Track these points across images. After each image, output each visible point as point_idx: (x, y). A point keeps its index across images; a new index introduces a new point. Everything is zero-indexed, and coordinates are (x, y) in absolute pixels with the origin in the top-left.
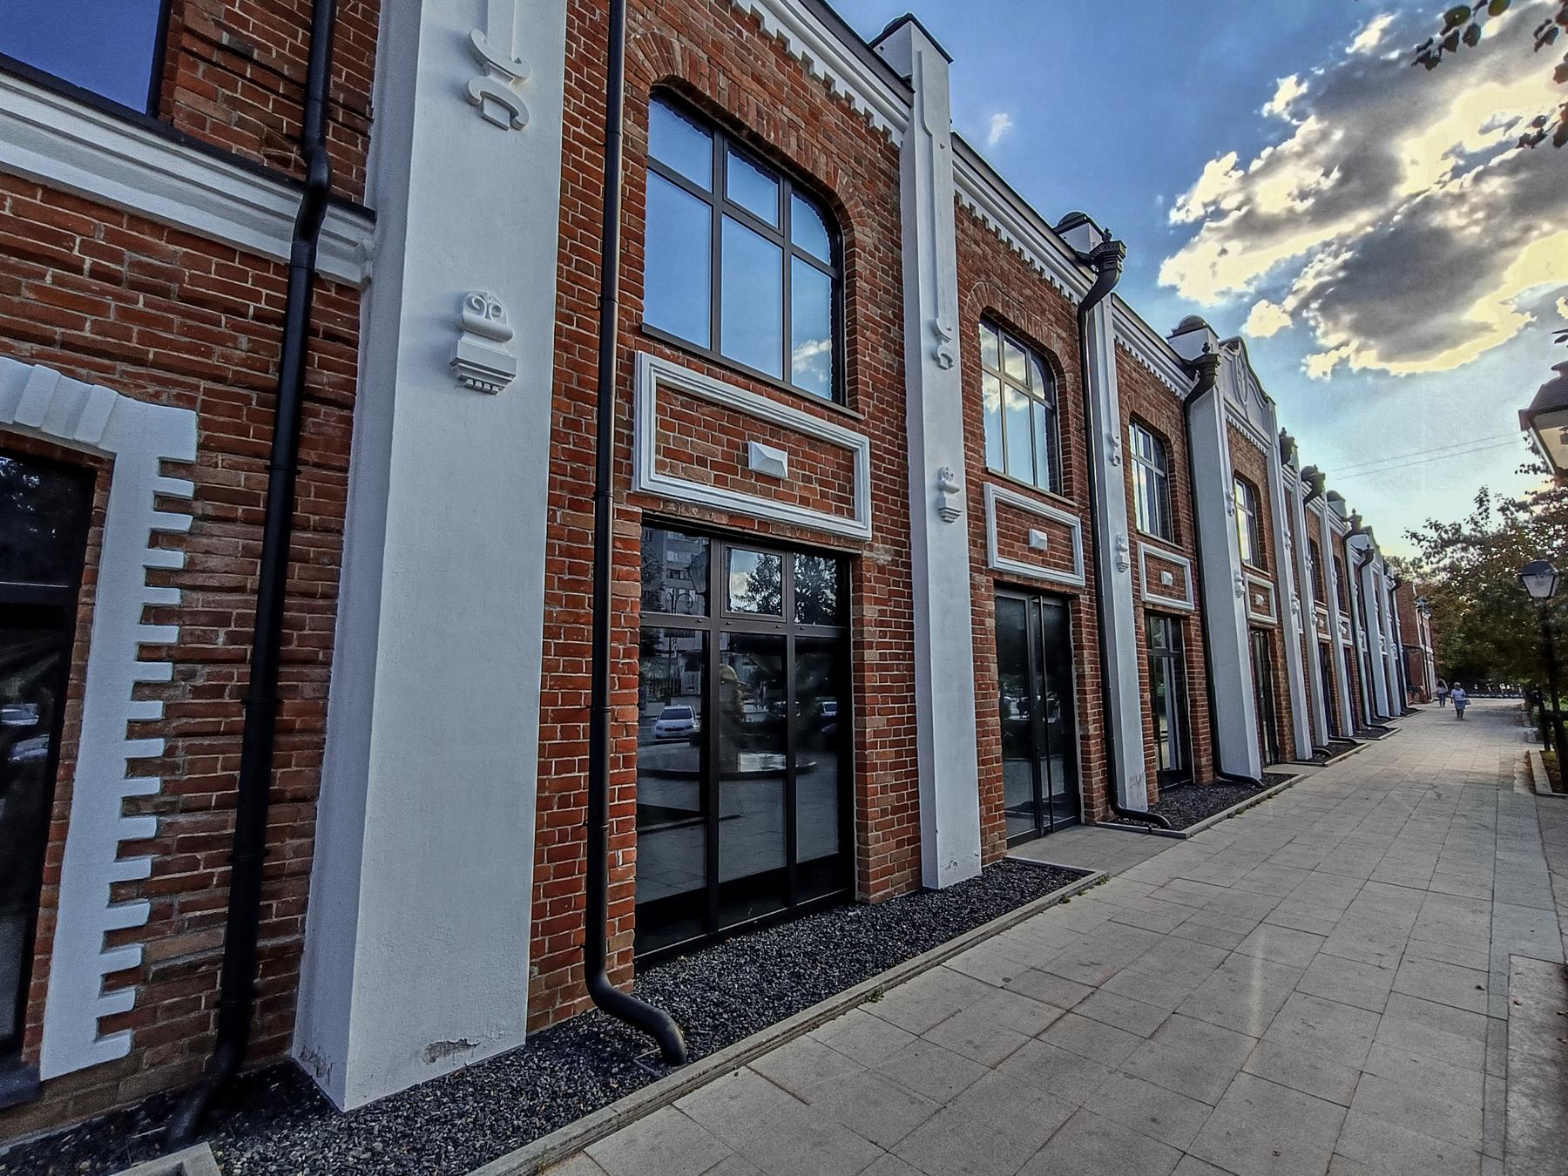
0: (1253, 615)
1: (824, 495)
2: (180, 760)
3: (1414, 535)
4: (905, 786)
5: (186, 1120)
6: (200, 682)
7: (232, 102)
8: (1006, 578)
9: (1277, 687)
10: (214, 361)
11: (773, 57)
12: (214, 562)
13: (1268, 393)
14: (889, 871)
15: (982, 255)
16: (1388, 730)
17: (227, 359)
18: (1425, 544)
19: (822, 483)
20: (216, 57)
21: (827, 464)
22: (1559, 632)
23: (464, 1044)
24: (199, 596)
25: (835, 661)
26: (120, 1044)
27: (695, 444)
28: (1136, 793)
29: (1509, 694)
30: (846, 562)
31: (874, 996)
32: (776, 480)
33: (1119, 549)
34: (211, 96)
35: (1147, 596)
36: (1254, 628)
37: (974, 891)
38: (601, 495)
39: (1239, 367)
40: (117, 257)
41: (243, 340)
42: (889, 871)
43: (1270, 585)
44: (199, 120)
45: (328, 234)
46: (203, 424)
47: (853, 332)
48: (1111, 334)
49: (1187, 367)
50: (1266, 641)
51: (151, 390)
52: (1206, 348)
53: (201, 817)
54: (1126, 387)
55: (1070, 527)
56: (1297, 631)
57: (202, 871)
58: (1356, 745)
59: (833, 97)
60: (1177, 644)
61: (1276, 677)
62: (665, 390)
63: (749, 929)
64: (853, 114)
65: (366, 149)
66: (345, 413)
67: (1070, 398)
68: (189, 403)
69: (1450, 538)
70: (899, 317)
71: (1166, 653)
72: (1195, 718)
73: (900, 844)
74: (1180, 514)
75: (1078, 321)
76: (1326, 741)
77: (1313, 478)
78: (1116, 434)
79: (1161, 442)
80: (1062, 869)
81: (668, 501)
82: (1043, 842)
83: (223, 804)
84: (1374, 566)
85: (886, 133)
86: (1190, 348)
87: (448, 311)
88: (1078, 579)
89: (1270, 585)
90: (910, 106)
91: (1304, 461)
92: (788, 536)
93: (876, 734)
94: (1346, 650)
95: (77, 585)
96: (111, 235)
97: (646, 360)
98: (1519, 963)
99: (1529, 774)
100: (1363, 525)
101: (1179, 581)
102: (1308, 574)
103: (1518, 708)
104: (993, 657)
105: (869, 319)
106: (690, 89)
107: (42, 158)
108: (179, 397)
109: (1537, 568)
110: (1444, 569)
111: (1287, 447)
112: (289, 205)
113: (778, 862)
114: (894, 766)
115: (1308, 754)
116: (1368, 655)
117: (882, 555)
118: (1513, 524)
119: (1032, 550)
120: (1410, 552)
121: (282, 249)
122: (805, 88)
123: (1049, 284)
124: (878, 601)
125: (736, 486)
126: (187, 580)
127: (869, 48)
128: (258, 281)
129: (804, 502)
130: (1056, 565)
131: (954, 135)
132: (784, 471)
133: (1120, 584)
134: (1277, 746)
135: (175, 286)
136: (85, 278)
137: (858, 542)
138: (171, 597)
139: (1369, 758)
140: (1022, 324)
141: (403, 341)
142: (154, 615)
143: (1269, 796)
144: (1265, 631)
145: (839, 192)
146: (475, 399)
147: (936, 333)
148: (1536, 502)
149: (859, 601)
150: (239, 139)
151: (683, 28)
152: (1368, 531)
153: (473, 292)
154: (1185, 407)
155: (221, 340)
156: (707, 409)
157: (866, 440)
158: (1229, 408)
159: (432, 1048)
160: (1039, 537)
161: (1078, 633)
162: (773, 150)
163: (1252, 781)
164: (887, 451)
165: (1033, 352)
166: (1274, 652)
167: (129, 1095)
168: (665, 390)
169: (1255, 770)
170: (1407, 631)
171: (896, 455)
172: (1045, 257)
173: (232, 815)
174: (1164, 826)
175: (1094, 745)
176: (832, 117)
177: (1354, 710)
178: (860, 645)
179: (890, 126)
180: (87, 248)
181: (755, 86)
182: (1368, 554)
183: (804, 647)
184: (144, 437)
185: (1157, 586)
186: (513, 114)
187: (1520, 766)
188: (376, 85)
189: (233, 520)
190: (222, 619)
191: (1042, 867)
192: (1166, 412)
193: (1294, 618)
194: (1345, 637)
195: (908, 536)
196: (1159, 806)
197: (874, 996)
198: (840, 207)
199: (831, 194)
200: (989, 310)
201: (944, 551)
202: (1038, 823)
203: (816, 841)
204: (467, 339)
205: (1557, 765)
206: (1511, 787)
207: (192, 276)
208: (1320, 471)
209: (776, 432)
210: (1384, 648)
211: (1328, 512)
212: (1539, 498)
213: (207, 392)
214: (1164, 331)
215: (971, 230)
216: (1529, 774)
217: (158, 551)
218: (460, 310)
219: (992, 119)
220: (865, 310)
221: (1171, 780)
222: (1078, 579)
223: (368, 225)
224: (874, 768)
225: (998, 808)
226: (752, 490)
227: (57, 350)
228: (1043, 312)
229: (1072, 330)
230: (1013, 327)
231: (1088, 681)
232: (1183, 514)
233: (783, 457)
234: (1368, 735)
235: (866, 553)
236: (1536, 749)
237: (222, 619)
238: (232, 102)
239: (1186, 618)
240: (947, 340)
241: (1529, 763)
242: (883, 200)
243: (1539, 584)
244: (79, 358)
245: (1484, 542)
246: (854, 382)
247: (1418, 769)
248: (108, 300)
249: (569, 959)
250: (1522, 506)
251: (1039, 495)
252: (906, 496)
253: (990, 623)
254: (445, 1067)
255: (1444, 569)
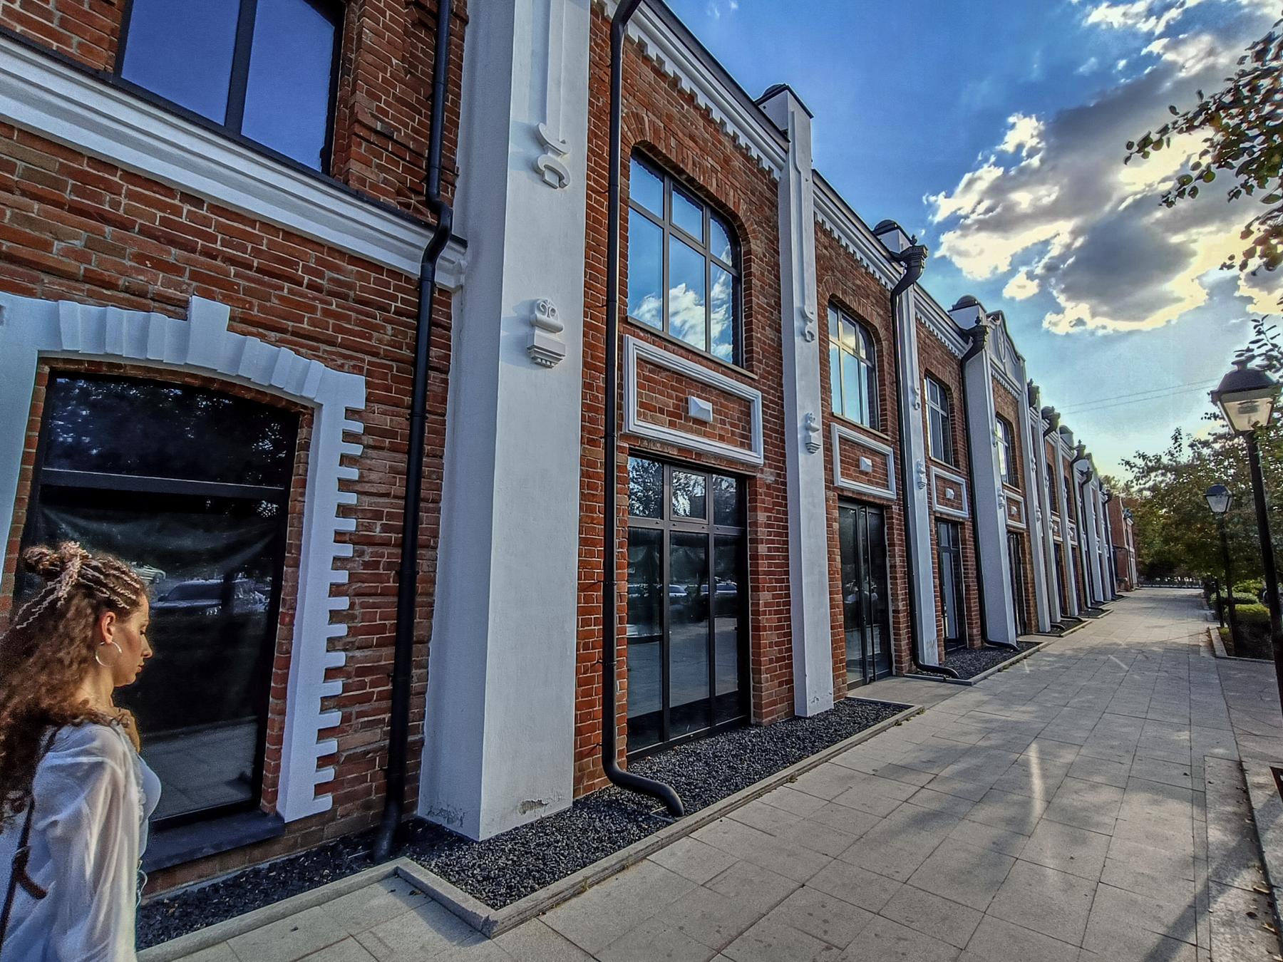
0: (1010, 522)
1: (733, 433)
2: (357, 612)
3: (1128, 463)
4: (782, 643)
5: (385, 845)
6: (367, 558)
7: (379, 166)
8: (845, 493)
9: (1026, 576)
10: (373, 343)
11: (701, 122)
12: (374, 476)
13: (1020, 349)
14: (774, 703)
15: (833, 261)
16: (1103, 611)
17: (380, 341)
18: (1136, 470)
19: (732, 425)
20: (373, 138)
21: (734, 410)
22: (1232, 538)
23: (540, 803)
24: (366, 499)
25: (738, 554)
26: (326, 802)
27: (660, 400)
28: (931, 653)
29: (1191, 585)
30: (744, 481)
31: (791, 779)
32: (704, 423)
33: (919, 472)
34: (368, 164)
35: (938, 508)
36: (1011, 532)
37: (832, 718)
38: (609, 436)
39: (999, 334)
40: (321, 276)
41: (389, 327)
42: (774, 703)
43: (1020, 499)
44: (362, 181)
45: (444, 259)
46: (368, 385)
47: (749, 316)
48: (913, 310)
49: (963, 334)
50: (1018, 539)
51: (340, 362)
52: (978, 321)
53: (368, 652)
54: (922, 349)
55: (884, 455)
56: (1040, 535)
57: (368, 690)
58: (1081, 622)
59: (738, 147)
60: (956, 543)
61: (1025, 569)
62: (642, 361)
63: (688, 740)
64: (748, 158)
65: (453, 195)
66: (443, 376)
67: (886, 360)
68: (359, 370)
69: (1153, 466)
70: (778, 304)
71: (947, 550)
72: (968, 599)
73: (781, 684)
74: (957, 444)
75: (891, 302)
76: (1059, 619)
77: (1050, 416)
78: (917, 385)
79: (945, 390)
80: (890, 705)
81: (643, 439)
82: (869, 688)
83: (381, 644)
84: (1093, 484)
85: (771, 171)
86: (966, 320)
87: (525, 313)
88: (890, 494)
89: (1020, 499)
90: (786, 152)
91: (1044, 402)
92: (712, 463)
93: (766, 605)
94: (1073, 549)
95: (37, 470)
96: (319, 261)
97: (631, 341)
98: (1211, 762)
99: (1211, 645)
100: (1086, 452)
101: (958, 496)
102: (1046, 490)
103: (1199, 596)
104: (837, 551)
105: (760, 306)
106: (652, 148)
107: (280, 211)
108: (354, 367)
109: (1217, 490)
110: (1149, 489)
111: (1033, 393)
112: (423, 239)
113: (656, 706)
114: (777, 628)
115: (1048, 629)
116: (1088, 552)
117: (768, 477)
118: (1199, 456)
119: (862, 472)
120: (1122, 476)
121: (413, 268)
122: (720, 142)
123: (872, 276)
124: (766, 510)
125: (682, 428)
126: (358, 488)
127: (755, 105)
128: (397, 288)
129: (722, 438)
130: (877, 484)
131: (814, 171)
132: (710, 418)
133: (919, 497)
134: (1026, 624)
135: (352, 293)
136: (304, 289)
137: (754, 467)
138: (351, 499)
139: (1091, 633)
140: (854, 306)
141: (502, 333)
142: (344, 511)
143: (1025, 657)
144: (1017, 534)
145: (743, 220)
146: (541, 372)
147: (804, 317)
148: (1215, 441)
149: (755, 509)
150: (385, 193)
151: (649, 106)
152: (1089, 456)
153: (541, 298)
154: (962, 364)
155: (376, 328)
156: (664, 374)
157: (759, 393)
158: (993, 365)
159: (524, 804)
160: (866, 463)
161: (891, 534)
162: (701, 188)
163: (1011, 647)
164: (771, 401)
165: (861, 326)
166: (1023, 550)
167: (330, 833)
168: (642, 361)
169: (1012, 639)
170: (1115, 535)
171: (777, 404)
172: (867, 252)
173: (390, 651)
174: (954, 676)
175: (903, 617)
176: (737, 163)
177: (1078, 596)
178: (755, 541)
179: (773, 166)
180: (307, 270)
181: (692, 144)
182: (1088, 475)
183: (720, 542)
184: (334, 393)
185: (944, 500)
186: (561, 178)
187: (1204, 638)
188: (459, 152)
189: (382, 448)
190: (377, 515)
191: (876, 703)
192: (949, 368)
193: (1038, 524)
194: (1072, 539)
195: (784, 462)
196: (946, 664)
197: (791, 779)
198: (741, 226)
199: (736, 217)
200: (833, 296)
201: (809, 470)
202: (865, 676)
203: (727, 684)
204: (538, 332)
205: (1230, 636)
206: (1198, 652)
207: (361, 286)
208: (1056, 411)
209: (705, 388)
210: (1099, 547)
211: (1060, 442)
212: (1218, 437)
213: (370, 363)
214: (947, 307)
215: (823, 239)
216: (1211, 645)
217: (343, 468)
218: (532, 312)
219: (836, 151)
220: (758, 300)
221: (954, 645)
222: (890, 494)
223: (462, 250)
224: (765, 629)
225: (841, 662)
226: (691, 431)
227: (288, 337)
228: (868, 297)
229: (886, 308)
230: (849, 308)
231: (898, 570)
232: (960, 445)
233: (708, 406)
234: (1089, 615)
235: (759, 475)
236: (1214, 626)
237: (377, 515)
238: (379, 166)
239: (962, 524)
240: (557, 152)
241: (1210, 636)
242: (768, 220)
243: (1217, 503)
244: (305, 342)
245: (1177, 470)
246: (750, 352)
247: (1129, 640)
248: (317, 303)
249: (591, 753)
250: (1206, 444)
251: (716, 365)
252: (783, 434)
253: (836, 526)
254: (532, 817)
255: (1149, 489)
